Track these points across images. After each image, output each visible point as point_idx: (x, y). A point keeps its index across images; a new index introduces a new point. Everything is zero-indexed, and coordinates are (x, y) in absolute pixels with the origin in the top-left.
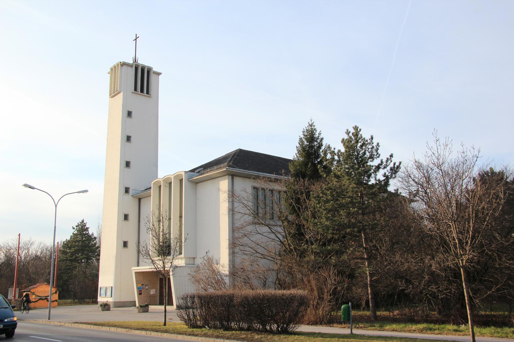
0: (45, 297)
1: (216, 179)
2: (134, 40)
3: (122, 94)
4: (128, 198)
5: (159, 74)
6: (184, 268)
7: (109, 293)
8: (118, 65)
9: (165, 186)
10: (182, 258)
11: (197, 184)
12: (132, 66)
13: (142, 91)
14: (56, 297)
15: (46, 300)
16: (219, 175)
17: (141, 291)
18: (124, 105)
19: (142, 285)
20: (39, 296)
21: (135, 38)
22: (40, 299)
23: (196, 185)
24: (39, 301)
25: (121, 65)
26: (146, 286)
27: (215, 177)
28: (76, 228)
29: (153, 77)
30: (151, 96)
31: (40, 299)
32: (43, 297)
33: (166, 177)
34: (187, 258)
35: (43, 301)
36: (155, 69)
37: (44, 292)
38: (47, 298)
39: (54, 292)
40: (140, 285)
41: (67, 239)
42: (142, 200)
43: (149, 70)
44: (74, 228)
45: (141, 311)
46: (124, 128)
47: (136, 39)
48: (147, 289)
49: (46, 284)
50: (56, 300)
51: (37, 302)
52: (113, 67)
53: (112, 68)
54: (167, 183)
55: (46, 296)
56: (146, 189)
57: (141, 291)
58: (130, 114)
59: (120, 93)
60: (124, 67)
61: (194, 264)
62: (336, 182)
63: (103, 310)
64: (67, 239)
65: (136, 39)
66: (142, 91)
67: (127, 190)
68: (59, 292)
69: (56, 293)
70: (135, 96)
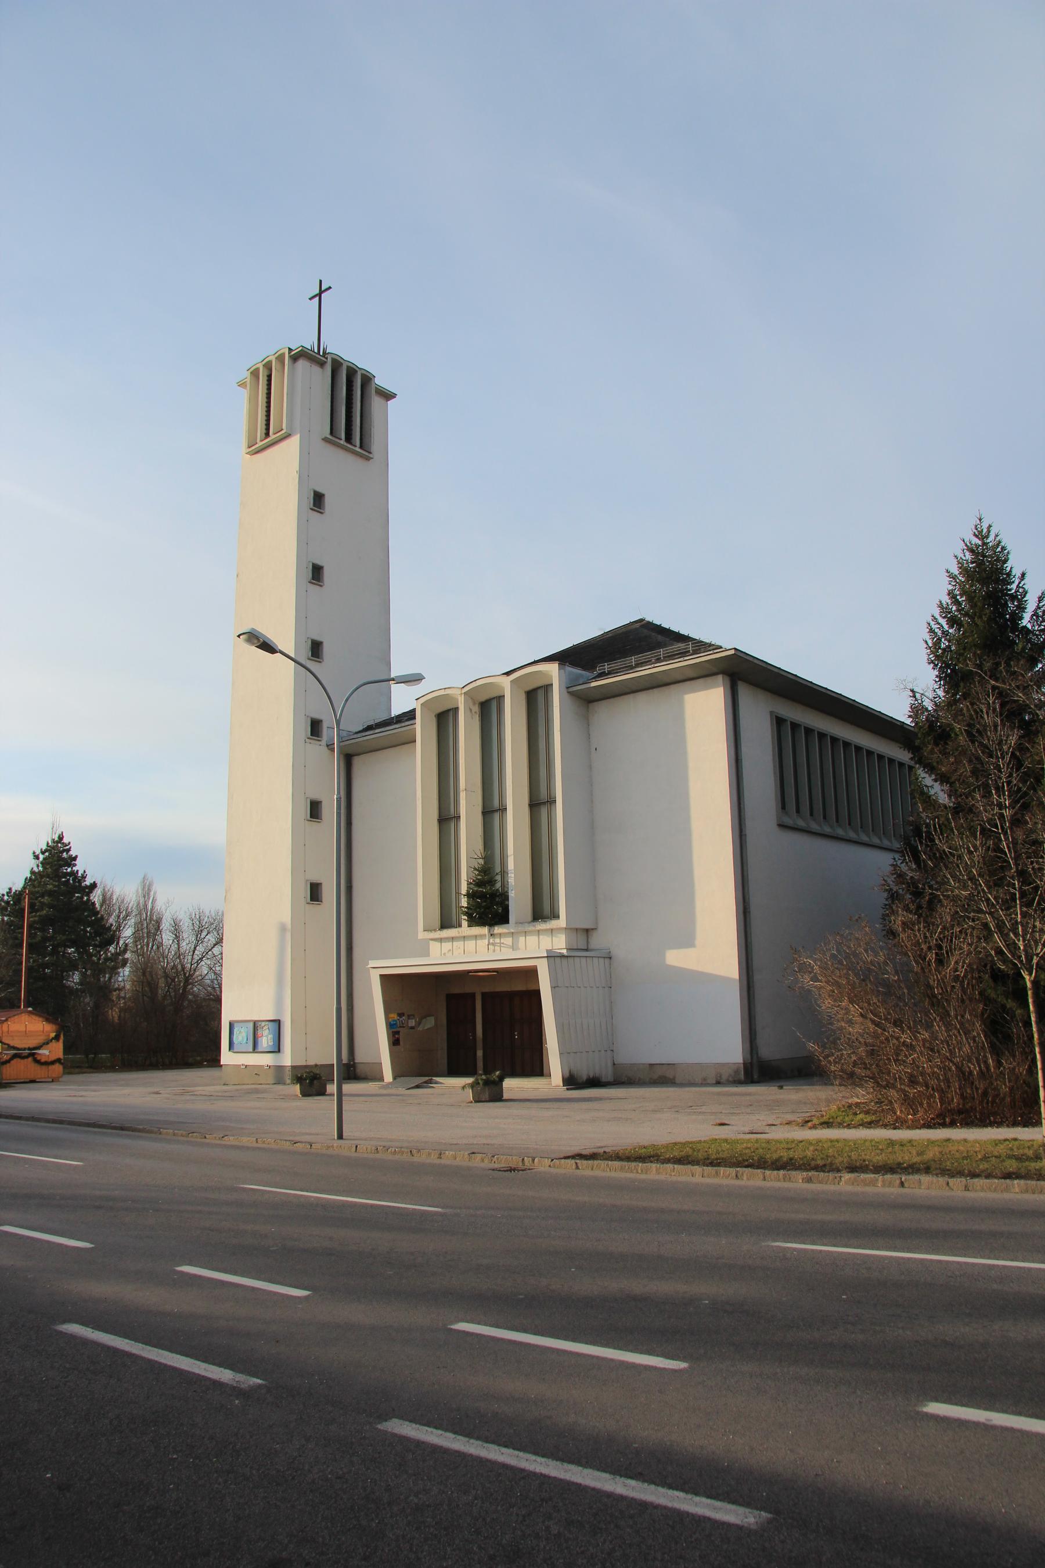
0: (29, 1049)
1: (673, 687)
2: (311, 299)
3: (295, 442)
4: (317, 749)
5: (388, 396)
6: (564, 961)
7: (266, 1040)
8: (280, 359)
9: (471, 710)
10: (559, 930)
11: (591, 705)
12: (322, 364)
13: (349, 438)
14: (55, 1050)
15: (30, 1059)
16: (692, 674)
17: (398, 1033)
18: (304, 475)
19: (400, 1015)
20: (14, 1048)
21: (317, 292)
22: (15, 1056)
23: (588, 707)
24: (12, 1062)
25: (290, 357)
26: (409, 1017)
27: (669, 681)
28: (41, 857)
29: (376, 402)
30: (371, 456)
31: (15, 1056)
32: (25, 1049)
33: (479, 683)
34: (571, 929)
35: (22, 1061)
36: (381, 381)
37: (26, 1034)
38: (34, 1054)
39: (53, 1035)
40: (394, 1016)
41: (10, 889)
42: (357, 761)
43: (367, 379)
44: (37, 857)
45: (486, 1096)
46: (304, 541)
47: (320, 295)
48: (412, 1028)
49: (30, 1012)
50: (58, 1061)
51: (8, 1065)
52: (273, 358)
53: (257, 370)
54: (474, 704)
55: (31, 1046)
56: (369, 728)
57: (398, 1033)
58: (318, 500)
59: (288, 436)
60: (302, 363)
61: (587, 950)
62: (1014, 707)
63: (305, 1094)
64: (10, 889)
65: (320, 295)
66: (349, 438)
67: (315, 727)
68: (64, 1035)
69: (57, 1038)
70: (330, 450)
